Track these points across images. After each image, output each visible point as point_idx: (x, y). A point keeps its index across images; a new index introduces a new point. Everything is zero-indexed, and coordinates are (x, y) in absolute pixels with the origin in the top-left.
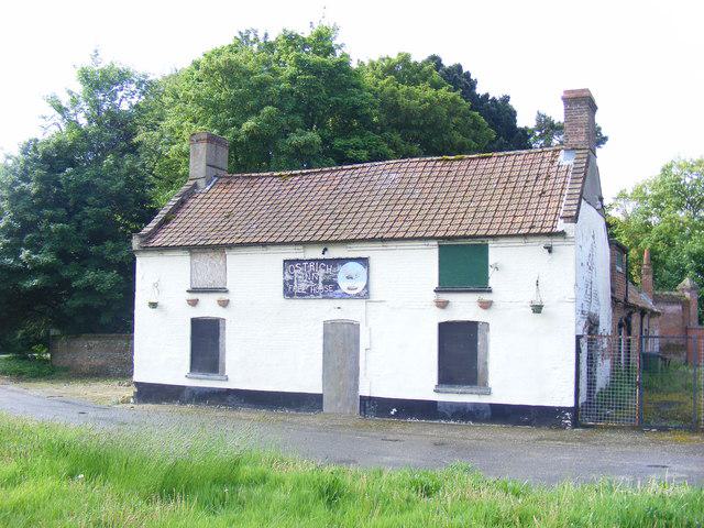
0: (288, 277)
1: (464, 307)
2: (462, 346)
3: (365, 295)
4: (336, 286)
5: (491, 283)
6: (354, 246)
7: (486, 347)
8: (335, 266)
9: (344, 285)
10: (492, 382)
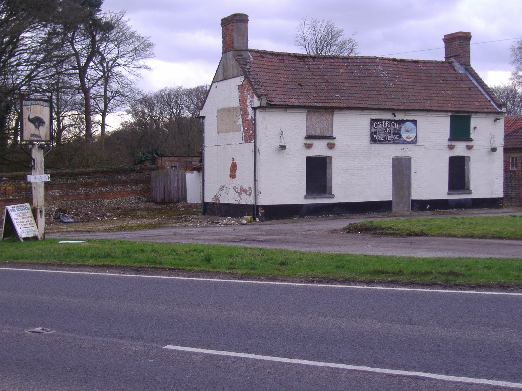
0: (374, 130)
1: (460, 149)
2: (122, 223)
3: (415, 142)
4: (400, 137)
5: (472, 136)
6: (412, 113)
7: (469, 169)
8: (400, 124)
9: (404, 135)
10: (472, 187)
